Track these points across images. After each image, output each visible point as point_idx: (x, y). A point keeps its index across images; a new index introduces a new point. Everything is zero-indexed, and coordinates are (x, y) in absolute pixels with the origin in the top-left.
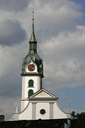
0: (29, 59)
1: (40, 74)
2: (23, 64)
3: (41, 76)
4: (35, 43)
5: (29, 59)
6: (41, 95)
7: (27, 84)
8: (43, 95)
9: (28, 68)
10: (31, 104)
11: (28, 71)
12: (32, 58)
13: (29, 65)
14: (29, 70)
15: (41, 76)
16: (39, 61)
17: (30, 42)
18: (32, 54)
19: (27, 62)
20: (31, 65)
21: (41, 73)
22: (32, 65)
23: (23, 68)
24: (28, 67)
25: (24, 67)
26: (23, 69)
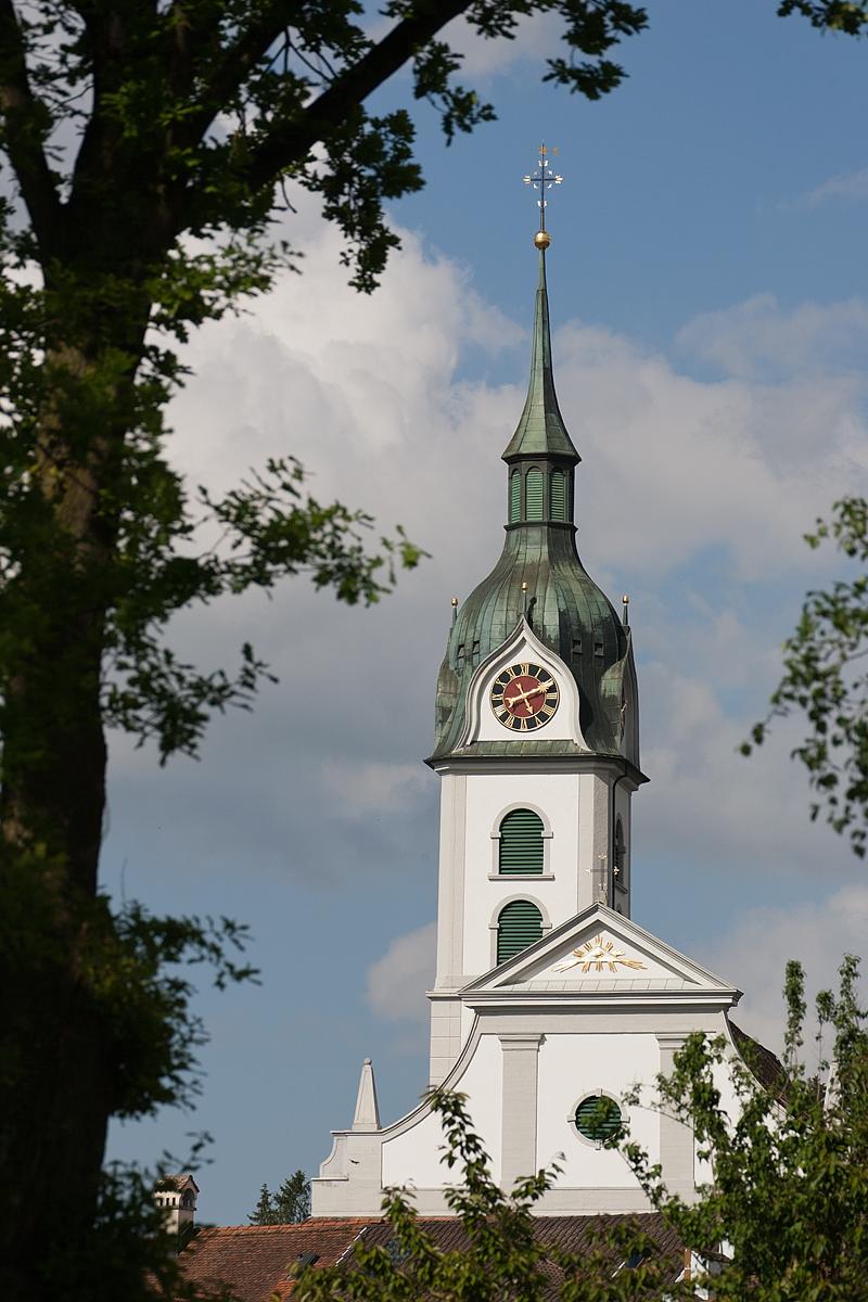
0: (496, 618)
1: (600, 758)
2: (446, 665)
3: (623, 773)
4: (562, 462)
5: (500, 617)
6: (586, 969)
7: (482, 850)
8: (599, 967)
9: (495, 704)
10: (490, 1048)
11: (492, 729)
12: (534, 601)
13: (504, 678)
14: (503, 718)
15: (623, 773)
16: (599, 632)
17: (513, 459)
18: (532, 573)
19: (484, 643)
20: (517, 669)
21: (619, 747)
22: (533, 669)
23: (448, 702)
24: (497, 689)
25: (460, 695)
26: (445, 712)
